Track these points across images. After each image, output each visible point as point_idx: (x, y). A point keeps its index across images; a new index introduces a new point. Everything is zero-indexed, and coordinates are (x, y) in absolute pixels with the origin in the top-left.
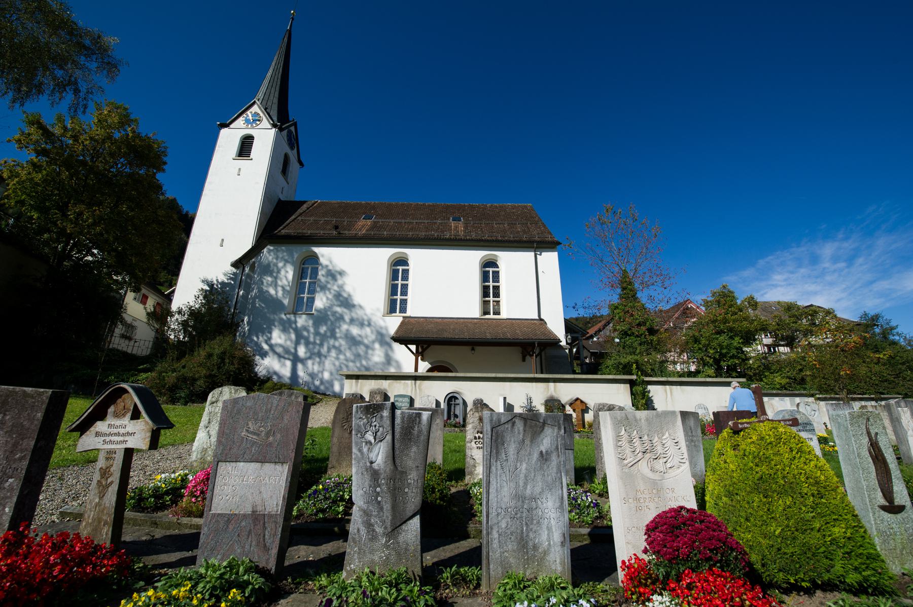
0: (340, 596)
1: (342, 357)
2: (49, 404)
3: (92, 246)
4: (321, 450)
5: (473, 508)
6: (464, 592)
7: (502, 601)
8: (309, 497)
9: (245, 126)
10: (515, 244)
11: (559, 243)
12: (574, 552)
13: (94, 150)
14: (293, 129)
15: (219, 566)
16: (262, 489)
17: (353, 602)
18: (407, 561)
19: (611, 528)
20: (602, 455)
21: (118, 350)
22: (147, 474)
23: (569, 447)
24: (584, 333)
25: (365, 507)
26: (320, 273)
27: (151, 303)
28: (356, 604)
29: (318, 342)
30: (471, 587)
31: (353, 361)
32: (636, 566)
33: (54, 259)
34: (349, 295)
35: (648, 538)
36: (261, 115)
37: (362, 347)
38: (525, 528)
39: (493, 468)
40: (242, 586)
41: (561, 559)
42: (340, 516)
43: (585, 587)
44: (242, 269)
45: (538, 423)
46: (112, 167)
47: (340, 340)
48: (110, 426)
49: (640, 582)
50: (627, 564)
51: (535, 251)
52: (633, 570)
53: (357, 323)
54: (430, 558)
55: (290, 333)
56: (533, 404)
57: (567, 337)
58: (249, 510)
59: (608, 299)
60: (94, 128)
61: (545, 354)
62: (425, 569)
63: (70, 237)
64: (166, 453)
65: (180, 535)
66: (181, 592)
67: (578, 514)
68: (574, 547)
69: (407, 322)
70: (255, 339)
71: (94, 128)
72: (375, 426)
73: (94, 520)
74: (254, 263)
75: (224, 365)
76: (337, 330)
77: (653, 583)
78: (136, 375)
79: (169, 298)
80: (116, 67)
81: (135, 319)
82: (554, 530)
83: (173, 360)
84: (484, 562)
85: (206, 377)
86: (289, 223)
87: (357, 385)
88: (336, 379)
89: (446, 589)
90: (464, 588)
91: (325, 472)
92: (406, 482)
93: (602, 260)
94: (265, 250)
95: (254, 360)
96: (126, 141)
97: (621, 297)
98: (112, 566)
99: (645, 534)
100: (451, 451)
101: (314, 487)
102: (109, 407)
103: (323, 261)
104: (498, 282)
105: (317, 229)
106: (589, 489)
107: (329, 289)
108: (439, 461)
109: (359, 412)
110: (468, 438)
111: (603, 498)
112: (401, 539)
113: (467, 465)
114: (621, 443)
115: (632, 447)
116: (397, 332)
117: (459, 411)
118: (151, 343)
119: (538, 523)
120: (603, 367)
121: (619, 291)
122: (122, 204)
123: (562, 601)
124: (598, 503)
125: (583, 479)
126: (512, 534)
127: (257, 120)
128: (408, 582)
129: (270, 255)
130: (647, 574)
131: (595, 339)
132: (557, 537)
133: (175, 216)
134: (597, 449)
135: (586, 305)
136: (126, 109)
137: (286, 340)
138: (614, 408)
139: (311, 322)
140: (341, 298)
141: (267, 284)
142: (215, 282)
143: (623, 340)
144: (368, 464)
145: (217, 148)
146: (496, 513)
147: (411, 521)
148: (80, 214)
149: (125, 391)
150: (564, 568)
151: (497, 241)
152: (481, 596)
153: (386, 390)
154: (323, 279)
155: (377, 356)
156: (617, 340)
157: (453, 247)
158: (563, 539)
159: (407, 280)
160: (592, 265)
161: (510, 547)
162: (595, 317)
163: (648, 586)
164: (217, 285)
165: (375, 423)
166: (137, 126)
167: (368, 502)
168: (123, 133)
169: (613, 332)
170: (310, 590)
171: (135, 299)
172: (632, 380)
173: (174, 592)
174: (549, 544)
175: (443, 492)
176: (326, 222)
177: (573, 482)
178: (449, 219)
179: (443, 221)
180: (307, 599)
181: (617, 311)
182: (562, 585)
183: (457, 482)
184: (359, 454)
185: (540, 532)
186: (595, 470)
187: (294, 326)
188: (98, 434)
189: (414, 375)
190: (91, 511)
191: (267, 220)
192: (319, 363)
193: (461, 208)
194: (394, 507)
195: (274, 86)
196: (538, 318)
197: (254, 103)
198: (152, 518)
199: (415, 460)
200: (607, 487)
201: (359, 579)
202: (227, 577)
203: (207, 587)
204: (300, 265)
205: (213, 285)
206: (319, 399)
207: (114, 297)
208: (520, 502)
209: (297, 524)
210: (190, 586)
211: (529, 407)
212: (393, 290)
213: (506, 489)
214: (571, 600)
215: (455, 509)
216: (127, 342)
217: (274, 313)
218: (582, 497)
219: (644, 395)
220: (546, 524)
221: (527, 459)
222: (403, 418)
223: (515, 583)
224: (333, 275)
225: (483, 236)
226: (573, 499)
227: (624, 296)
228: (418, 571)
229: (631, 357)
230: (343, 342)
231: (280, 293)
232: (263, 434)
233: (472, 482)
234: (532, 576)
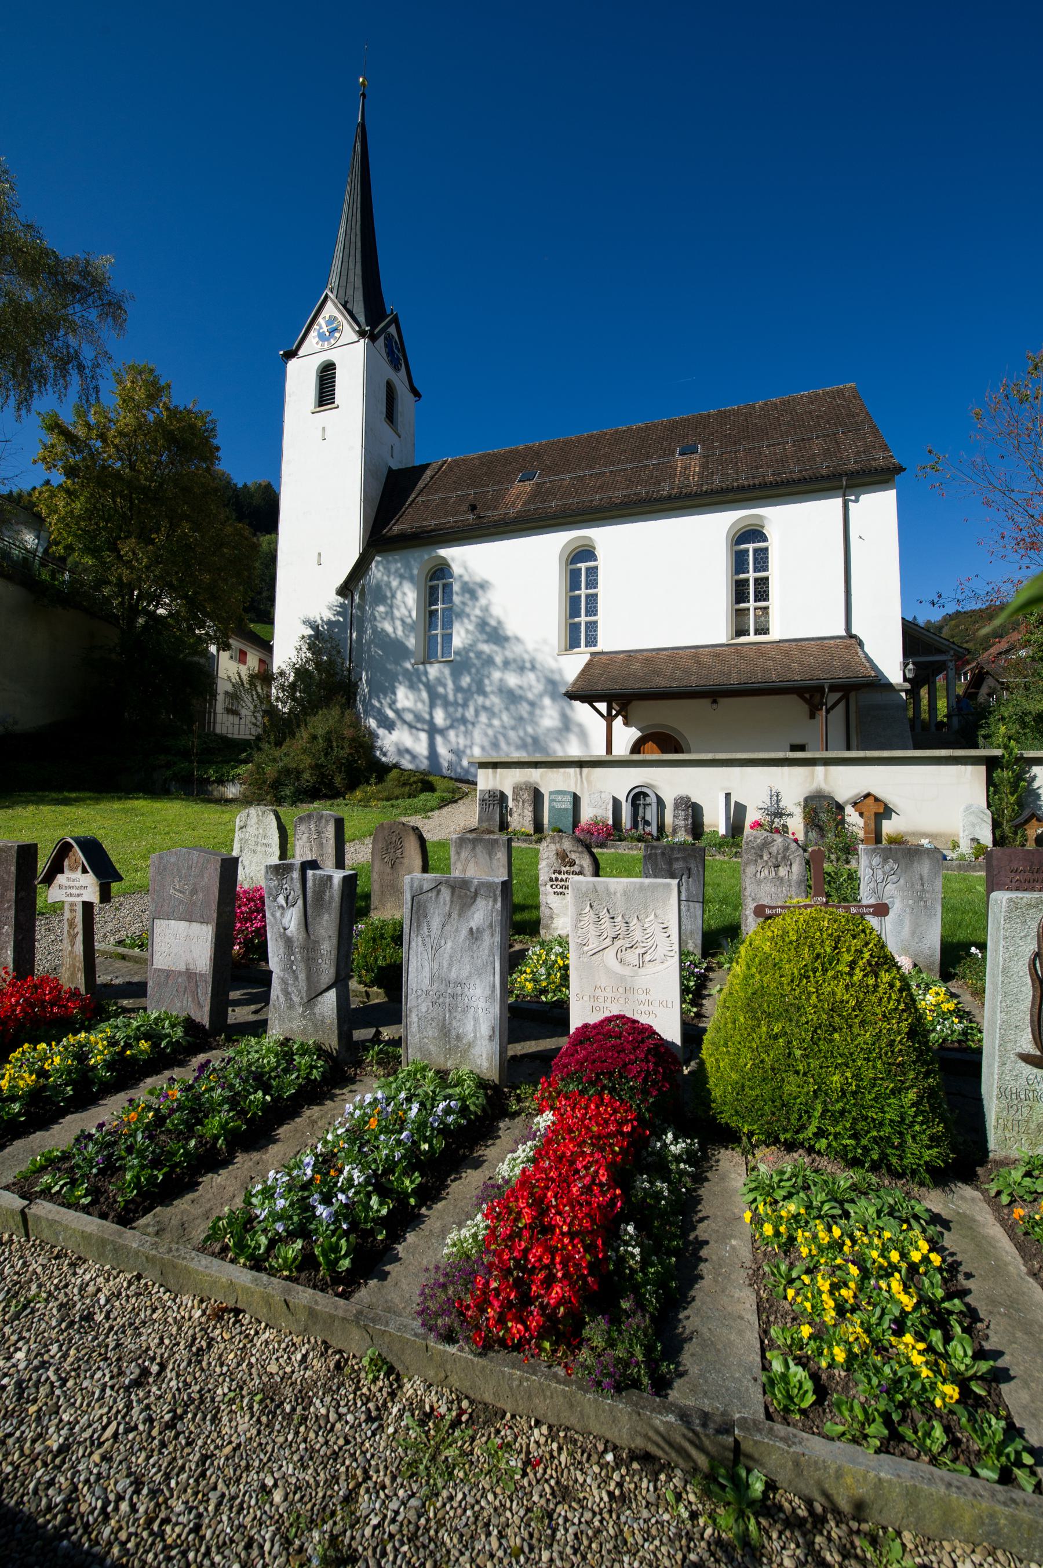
1: (496, 722)
2: (18, 858)
10: (801, 488)
11: (899, 469)
14: (392, 330)
29: (460, 701)
31: (513, 728)
34: (499, 622)
36: (340, 318)
53: (513, 666)
55: (419, 690)
56: (782, 804)
71: (123, 414)
76: (487, 682)
80: (120, 307)
87: (495, 777)
103: (456, 569)
112: (317, 1010)
117: (651, 814)
119: (463, 1011)
132: (485, 1030)
136: (152, 371)
139: (447, 671)
140: (488, 629)
145: (287, 399)
155: (549, 717)
166: (169, 398)
172: (996, 757)
178: (673, 453)
179: (662, 460)
187: (424, 679)
188: (60, 887)
193: (701, 423)
194: (309, 978)
196: (843, 633)
212: (573, 607)
222: (314, 880)
224: (471, 591)
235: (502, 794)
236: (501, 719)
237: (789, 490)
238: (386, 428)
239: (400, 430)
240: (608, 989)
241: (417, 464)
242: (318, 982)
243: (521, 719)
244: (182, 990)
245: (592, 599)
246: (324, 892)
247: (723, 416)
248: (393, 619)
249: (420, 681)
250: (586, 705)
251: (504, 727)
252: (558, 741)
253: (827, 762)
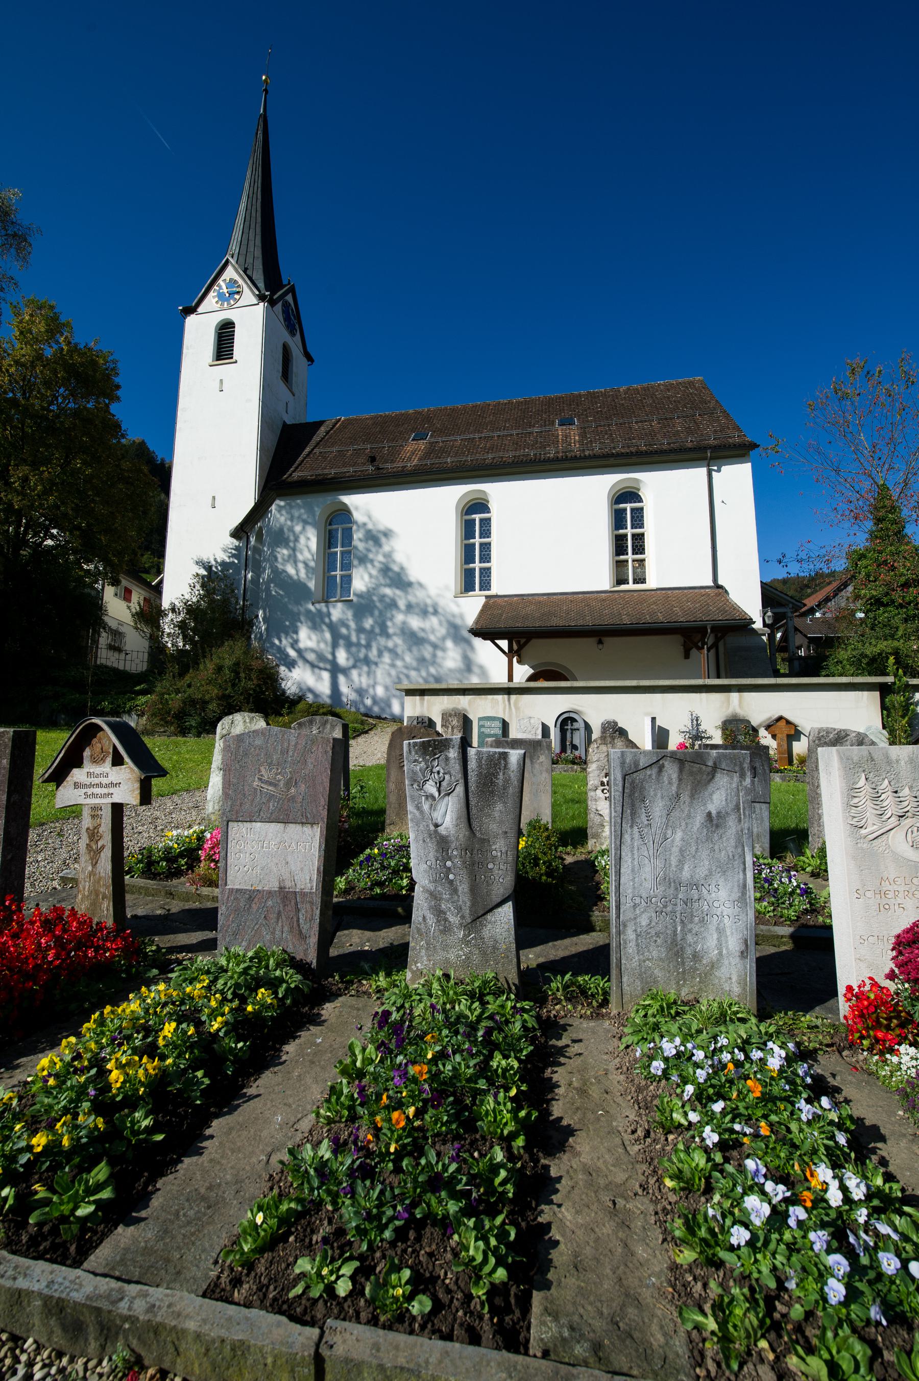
0: (402, 1006)
1: (399, 663)
2: (13, 747)
3: (50, 525)
4: (377, 799)
5: (600, 888)
6: (583, 1012)
7: (640, 1031)
8: (361, 865)
9: (219, 305)
10: (672, 457)
11: (754, 446)
12: (762, 963)
13: (24, 380)
14: (289, 298)
15: (244, 956)
16: (289, 859)
17: (419, 1015)
18: (497, 964)
19: (830, 928)
20: (820, 811)
21: (106, 667)
22: (158, 828)
23: (759, 799)
24: (797, 605)
25: (431, 887)
26: (355, 537)
27: (138, 596)
28: (424, 1019)
29: (363, 642)
30: (595, 1004)
31: (417, 669)
32: (872, 996)
33: (8, 547)
34: (402, 568)
35: (897, 957)
36: (240, 282)
37: (430, 649)
38: (679, 929)
39: (627, 837)
40: (273, 984)
41: (739, 976)
42: (404, 892)
43: (780, 1019)
44: (245, 539)
45: (704, 767)
46: (51, 403)
48: (89, 774)
49: (877, 1021)
50: (856, 990)
51: (709, 466)
52: (866, 1003)
53: (417, 610)
54: (533, 957)
55: (322, 631)
56: (702, 728)
57: (764, 614)
58: (274, 885)
59: (846, 542)
60: (18, 346)
61: (725, 644)
62: (524, 975)
63: (19, 514)
64: (179, 802)
65: (201, 909)
66: (195, 990)
67: (773, 904)
68: (764, 954)
69: (492, 605)
70: (277, 642)
71: (18, 346)
72: (438, 773)
73: (90, 893)
74: (261, 529)
75: (240, 681)
76: (389, 624)
77: (902, 1025)
78: (133, 699)
79: (158, 590)
80: (26, 240)
81: (121, 623)
82: (728, 934)
83: (174, 677)
84: (614, 972)
85: (219, 698)
86: (302, 461)
88: (394, 696)
89: (556, 1004)
90: (583, 1004)
91: (383, 830)
92: (489, 854)
93: (837, 471)
94: (273, 507)
95: (278, 672)
96: (60, 357)
97: (873, 536)
98: (116, 950)
99: (892, 950)
100: (566, 802)
101: (368, 851)
102: (83, 750)
103: (358, 516)
104: (642, 526)
105: (344, 466)
106: (795, 865)
107: (372, 561)
108: (546, 817)
109: (413, 753)
110: (590, 783)
111: (819, 880)
112: (486, 932)
113: (590, 824)
114: (856, 800)
115: (877, 807)
116: (478, 621)
117: (578, 739)
118: (146, 655)
119: (702, 921)
120: (831, 662)
121: (869, 525)
122: (74, 458)
123: (739, 1041)
124: (809, 888)
125: (785, 849)
126: (657, 935)
127: (235, 292)
128: (498, 993)
129: (282, 515)
130: (891, 1012)
131: (818, 615)
132: (733, 943)
133: (145, 469)
134: (811, 802)
135: (803, 555)
136: (52, 308)
137: (318, 642)
138: (847, 735)
139: (350, 614)
140: (390, 574)
141: (283, 559)
143: (871, 615)
144: (432, 828)
145: (185, 351)
146: (632, 904)
147: (500, 909)
148: (25, 480)
149: (99, 729)
150: (744, 989)
151: (639, 454)
152: (610, 1018)
153: (466, 710)
154: (361, 546)
155: (451, 659)
156: (861, 615)
157: (734, 459)
158: (743, 948)
159: (489, 537)
160: (817, 481)
161: (655, 954)
162: (819, 575)
163: (893, 1030)
164: (216, 567)
165: (437, 769)
166: (71, 333)
167: (435, 881)
168: (55, 347)
169: (854, 602)
170: (364, 993)
171: (116, 595)
173: (188, 990)
174: (720, 954)
175: (551, 864)
176: (357, 452)
177: (767, 854)
178: (553, 423)
180: (360, 1005)
181: (864, 562)
182: (739, 1015)
183: (575, 847)
184: (417, 813)
185: (705, 934)
186: (807, 836)
187: (327, 620)
188: (77, 785)
189: (506, 686)
190: (85, 882)
191: (270, 459)
192: (369, 674)
193: (574, 401)
194: (474, 890)
195: (253, 226)
197: (227, 263)
198: (166, 886)
199: (501, 822)
200: (826, 863)
201: (428, 985)
202: (252, 972)
203: (229, 985)
204: (326, 526)
206: (372, 724)
207: (90, 594)
208: (672, 888)
209: (348, 901)
210: (207, 981)
211: (694, 732)
212: (468, 554)
213: (648, 869)
214: (753, 1041)
215: (573, 888)
216: (116, 655)
217: (298, 603)
218: (781, 877)
219: (908, 710)
220: (715, 923)
221: (683, 824)
222: (479, 760)
223: (661, 1007)
224: (375, 538)
225: (614, 448)
226: (766, 880)
227: (879, 534)
228: (513, 977)
229: (885, 643)
230: (398, 641)
231: (303, 574)
232: (282, 784)
233: (598, 849)
234: (691, 997)
235: (430, 720)
237: (665, 458)
238: (282, 385)
239: (294, 389)
240: (899, 881)
242: (489, 894)
244: (273, 916)
245: (485, 548)
246: (495, 775)
247: (593, 396)
248: (295, 562)
250: (489, 642)
253: (741, 689)
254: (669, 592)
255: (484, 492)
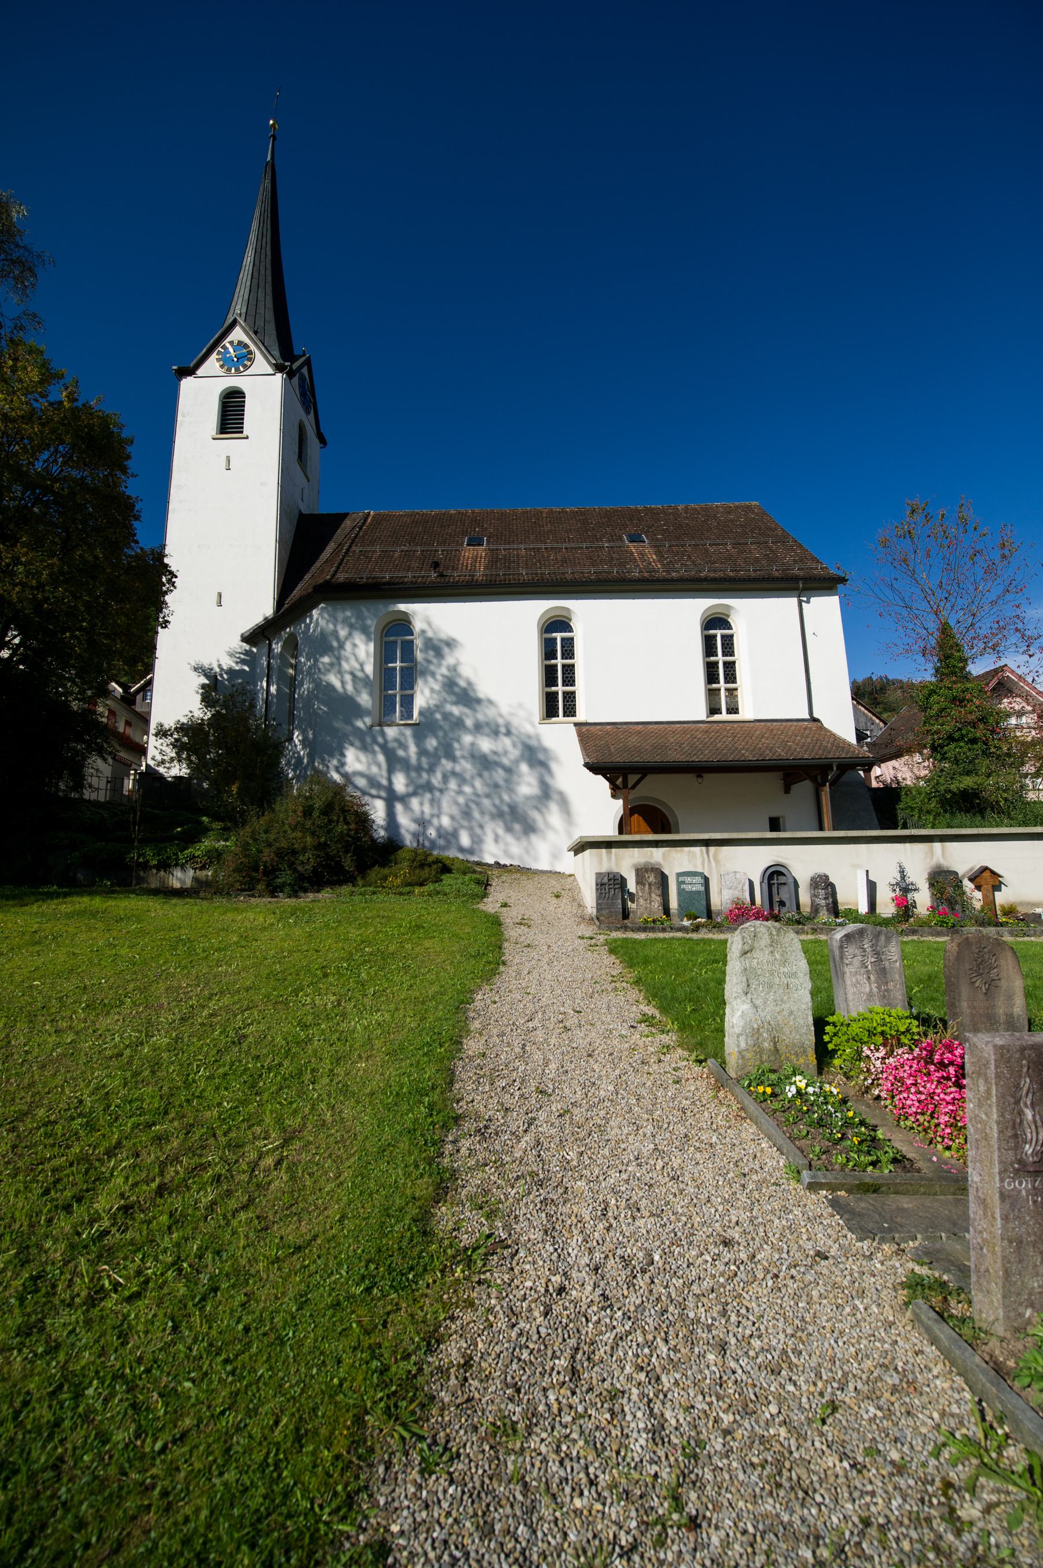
1: (467, 789)
11: (843, 580)
14: (305, 371)
29: (425, 766)
31: (488, 796)
34: (469, 683)
47: (463, 762)
51: (799, 596)
53: (487, 730)
55: (374, 752)
76: (456, 745)
87: (610, 858)
103: (418, 625)
127: (242, 361)
137: (369, 765)
140: (456, 689)
142: (217, 670)
153: (660, 864)
178: (621, 539)
187: (380, 740)
192: (432, 801)
193: (633, 515)
195: (262, 284)
205: (216, 677)
212: (549, 676)
224: (438, 647)
236: (473, 786)
241: (323, 510)
243: (496, 786)
249: (375, 741)
250: (600, 777)
251: (477, 795)
252: (539, 810)
253: (943, 839)
254: (769, 724)
255: (568, 610)
